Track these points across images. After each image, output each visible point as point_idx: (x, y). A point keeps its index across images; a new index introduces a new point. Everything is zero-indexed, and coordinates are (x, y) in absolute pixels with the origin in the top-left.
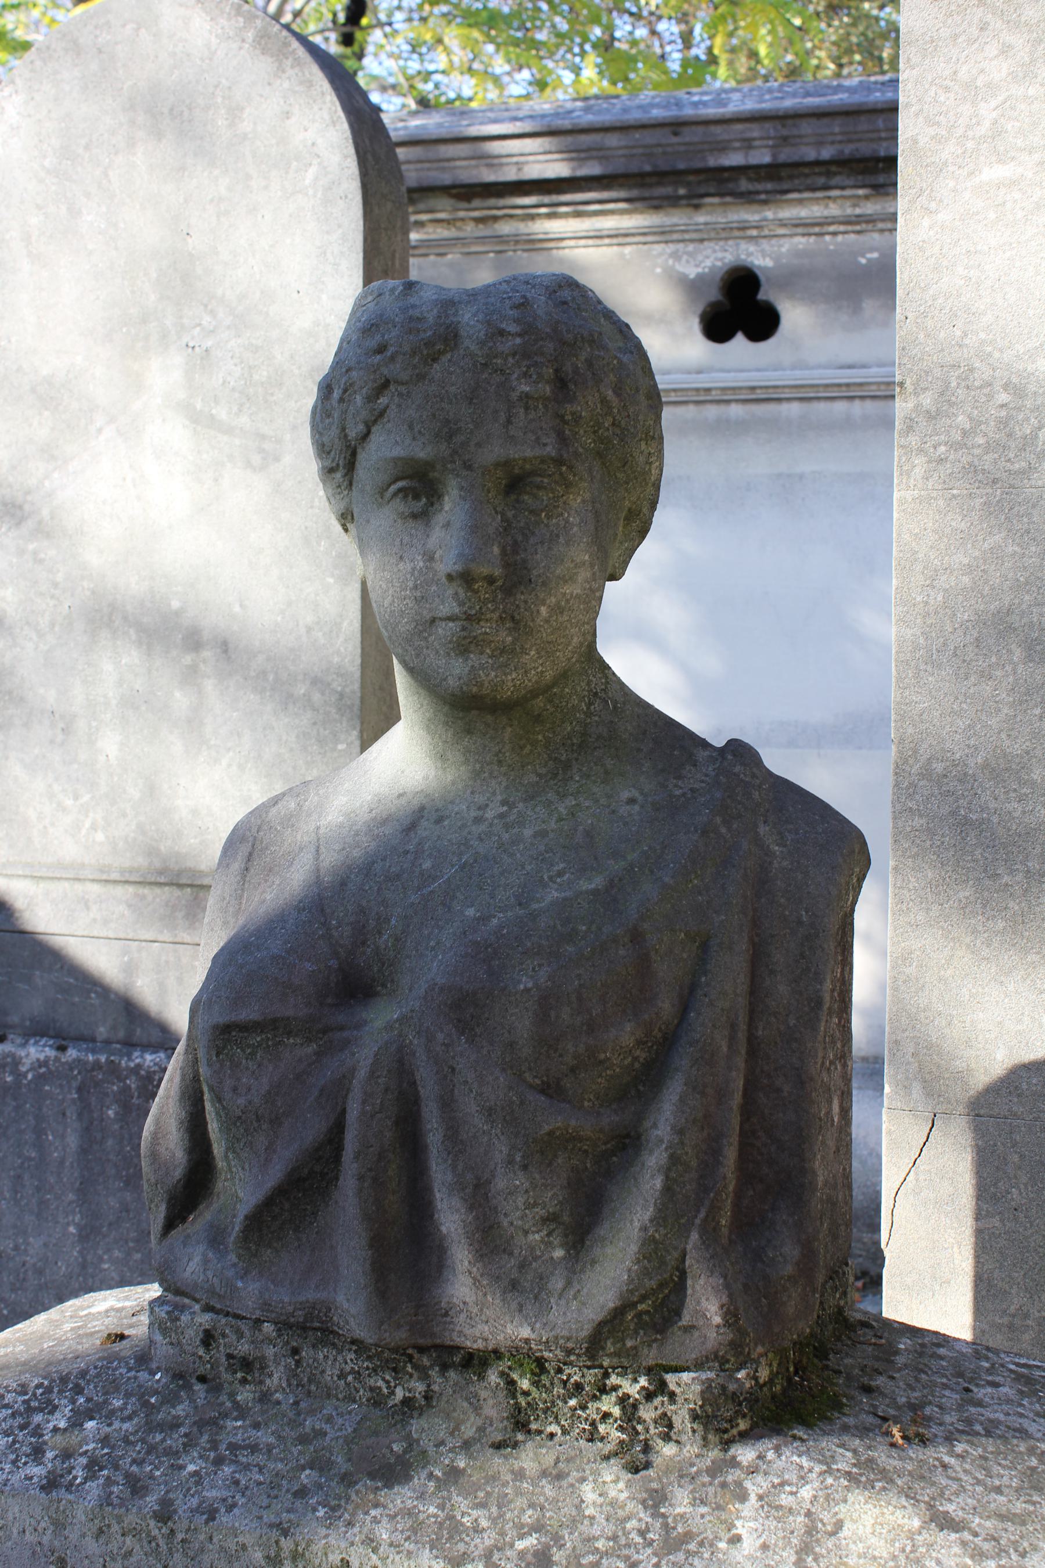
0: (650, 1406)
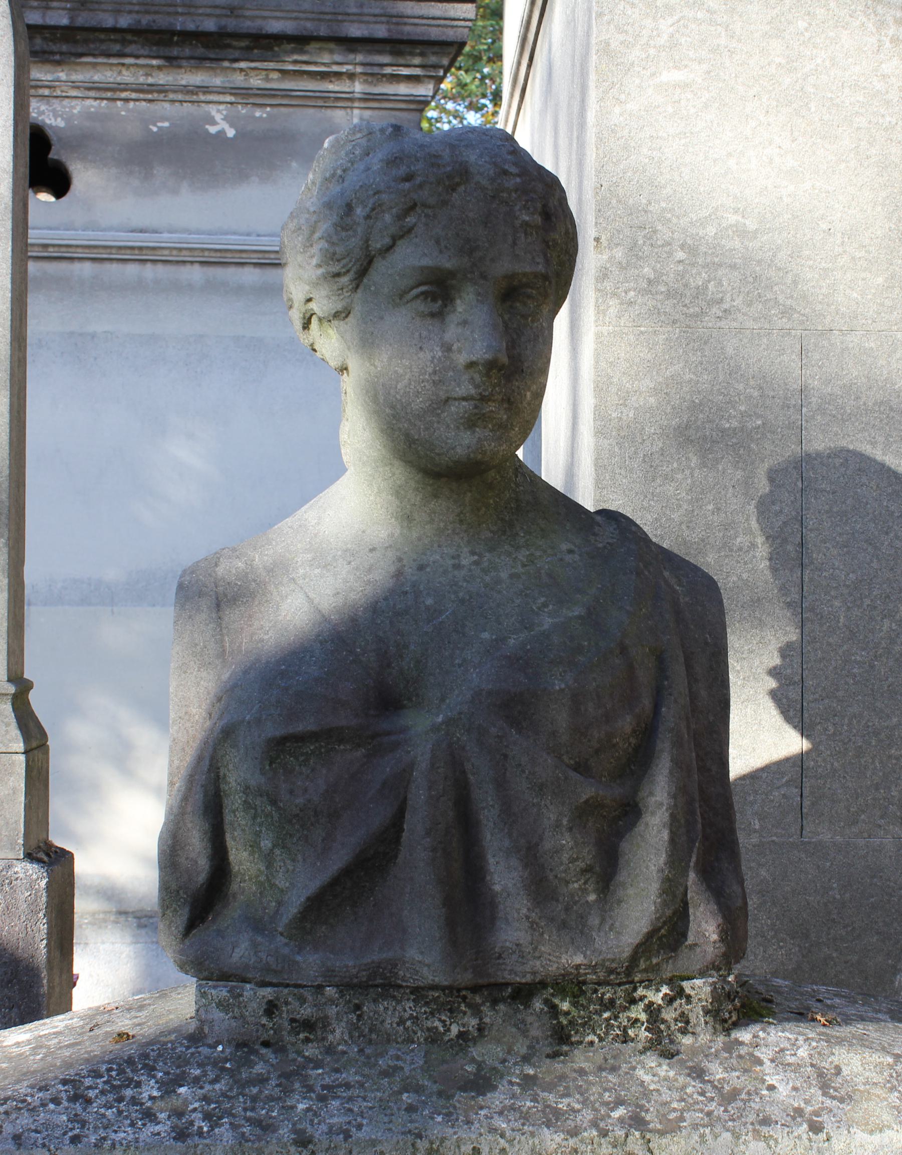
0: (671, 1008)
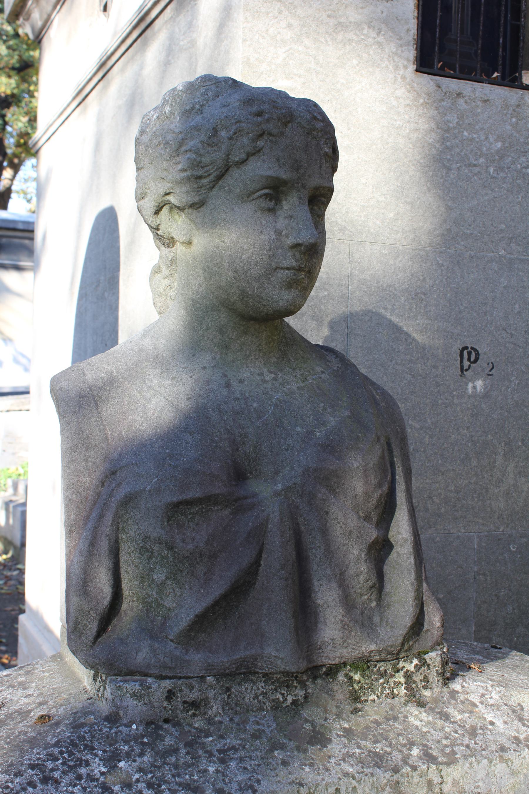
0: (419, 673)
